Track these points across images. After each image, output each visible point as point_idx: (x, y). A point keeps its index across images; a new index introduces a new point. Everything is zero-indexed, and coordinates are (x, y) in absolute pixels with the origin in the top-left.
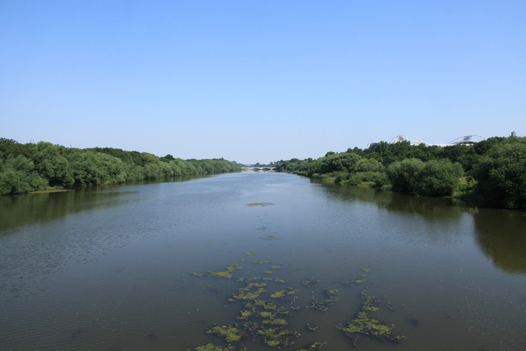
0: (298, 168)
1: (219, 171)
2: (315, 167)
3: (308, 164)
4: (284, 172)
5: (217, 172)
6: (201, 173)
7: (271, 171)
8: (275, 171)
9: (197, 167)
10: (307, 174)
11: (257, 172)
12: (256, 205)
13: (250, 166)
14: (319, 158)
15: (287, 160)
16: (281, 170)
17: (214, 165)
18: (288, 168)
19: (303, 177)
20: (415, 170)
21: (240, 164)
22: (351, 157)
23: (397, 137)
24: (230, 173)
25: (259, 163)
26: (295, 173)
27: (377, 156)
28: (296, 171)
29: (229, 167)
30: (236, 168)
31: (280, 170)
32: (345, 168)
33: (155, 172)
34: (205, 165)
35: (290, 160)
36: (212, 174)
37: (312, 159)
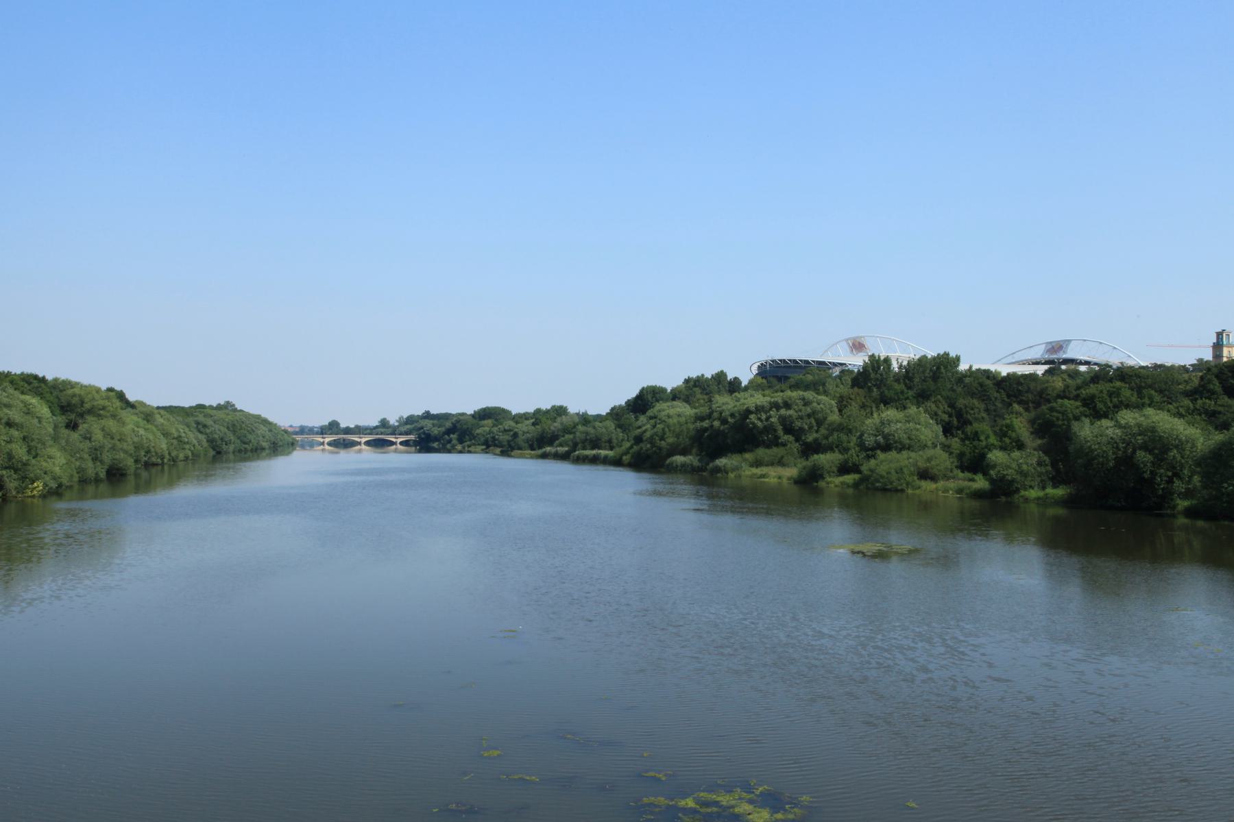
1: (245, 449)
2: (668, 434)
7: (396, 449)
20: (1172, 445)
22: (807, 403)
23: (845, 343)
27: (864, 401)
32: (791, 438)
33: (122, 449)
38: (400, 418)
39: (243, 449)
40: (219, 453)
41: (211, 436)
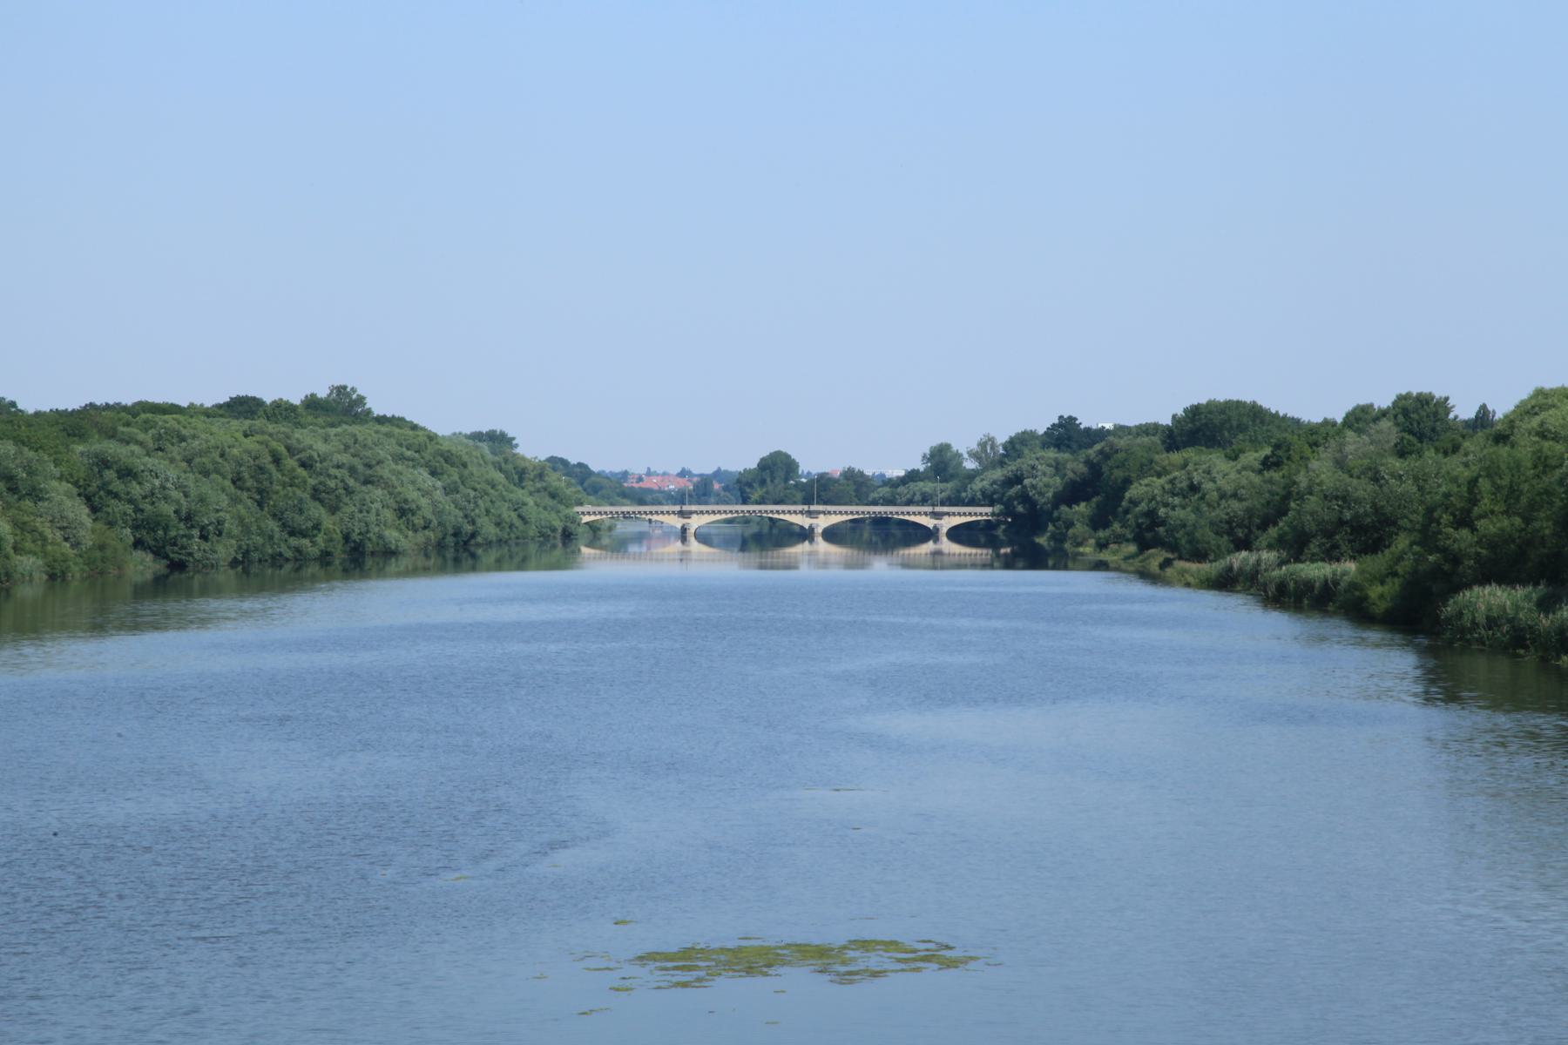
0: (1264, 526)
2: (1486, 503)
3: (1397, 464)
4: (1100, 566)
5: (277, 560)
6: (76, 570)
8: (983, 553)
9: (28, 503)
10: (1380, 594)
11: (762, 567)
12: (750, 971)
13: (680, 498)
14: (1540, 393)
15: (1132, 421)
16: (1059, 539)
17: (237, 481)
18: (1151, 514)
19: (1341, 629)
21: (557, 463)
24: (442, 569)
25: (795, 456)
26: (1225, 583)
28: (1240, 559)
29: (424, 502)
30: (509, 515)
31: (1042, 540)
34: (127, 473)
35: (1166, 420)
36: (219, 591)
37: (1443, 406)
38: (983, 445)
39: (289, 554)
40: (178, 566)
41: (148, 507)
